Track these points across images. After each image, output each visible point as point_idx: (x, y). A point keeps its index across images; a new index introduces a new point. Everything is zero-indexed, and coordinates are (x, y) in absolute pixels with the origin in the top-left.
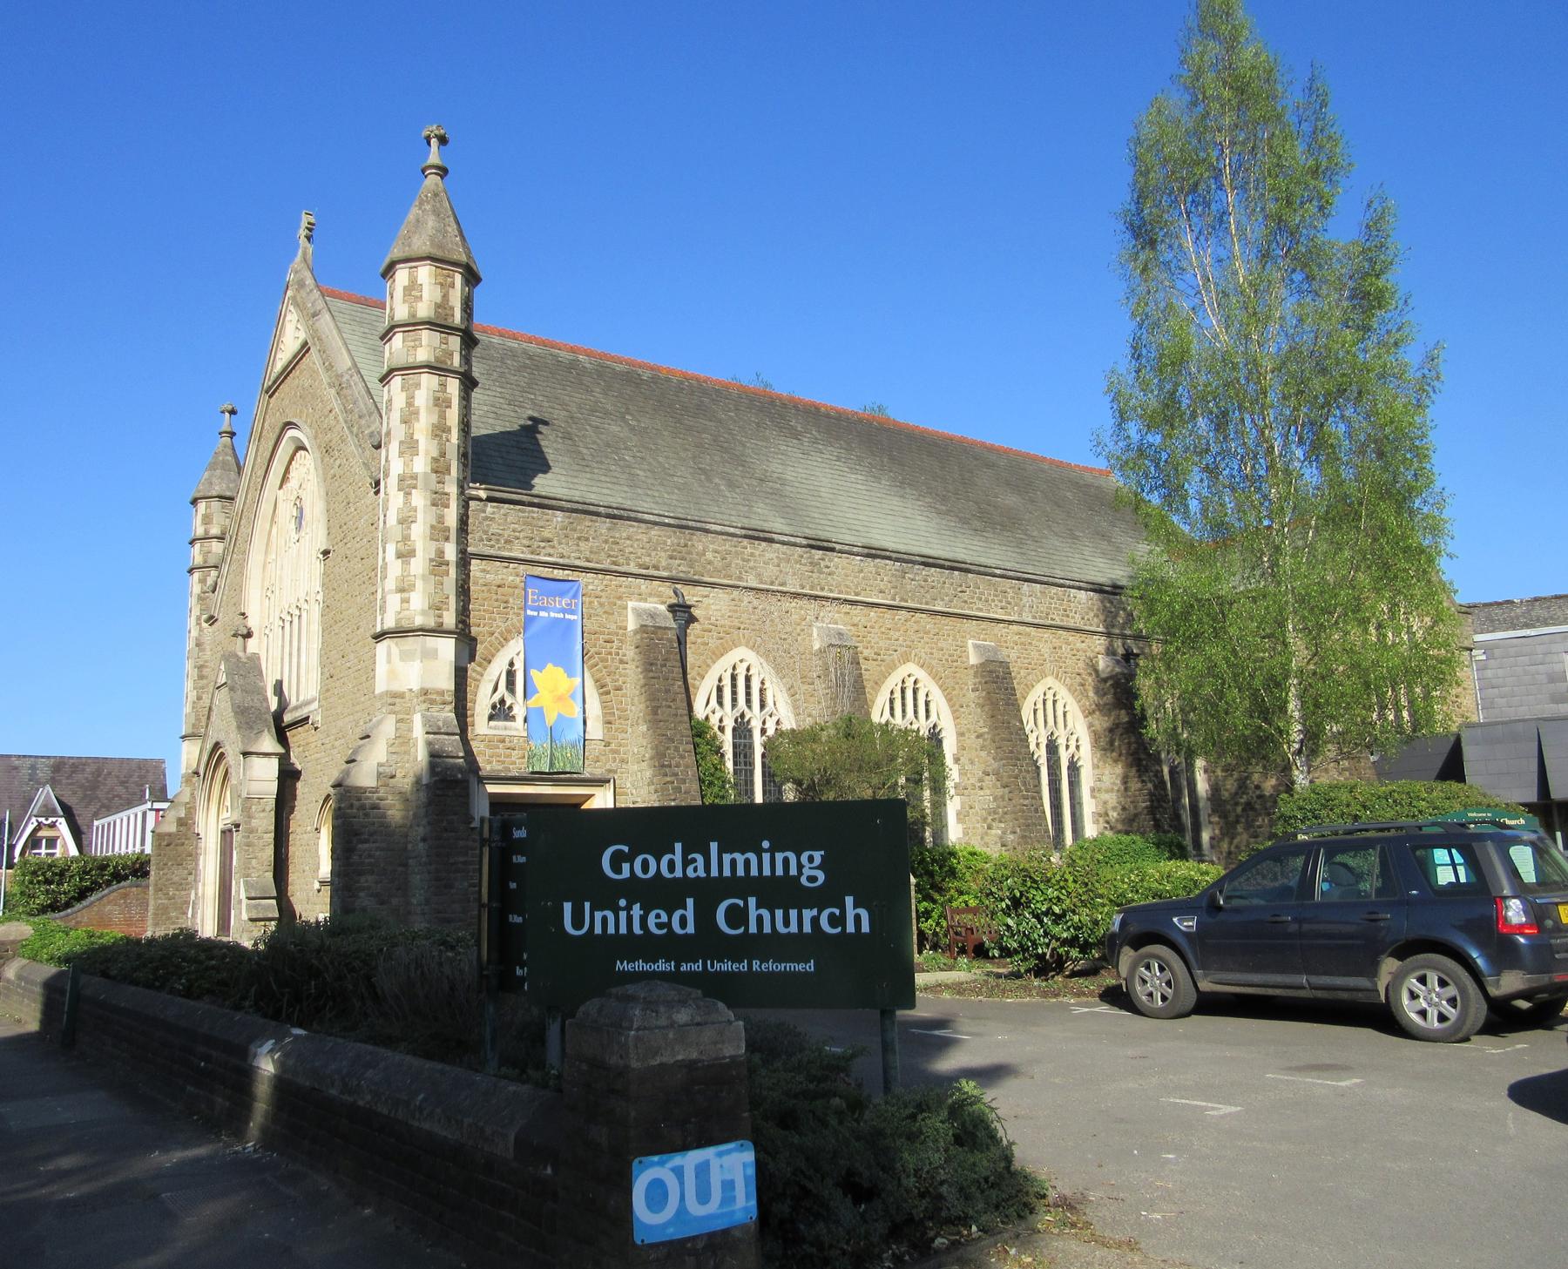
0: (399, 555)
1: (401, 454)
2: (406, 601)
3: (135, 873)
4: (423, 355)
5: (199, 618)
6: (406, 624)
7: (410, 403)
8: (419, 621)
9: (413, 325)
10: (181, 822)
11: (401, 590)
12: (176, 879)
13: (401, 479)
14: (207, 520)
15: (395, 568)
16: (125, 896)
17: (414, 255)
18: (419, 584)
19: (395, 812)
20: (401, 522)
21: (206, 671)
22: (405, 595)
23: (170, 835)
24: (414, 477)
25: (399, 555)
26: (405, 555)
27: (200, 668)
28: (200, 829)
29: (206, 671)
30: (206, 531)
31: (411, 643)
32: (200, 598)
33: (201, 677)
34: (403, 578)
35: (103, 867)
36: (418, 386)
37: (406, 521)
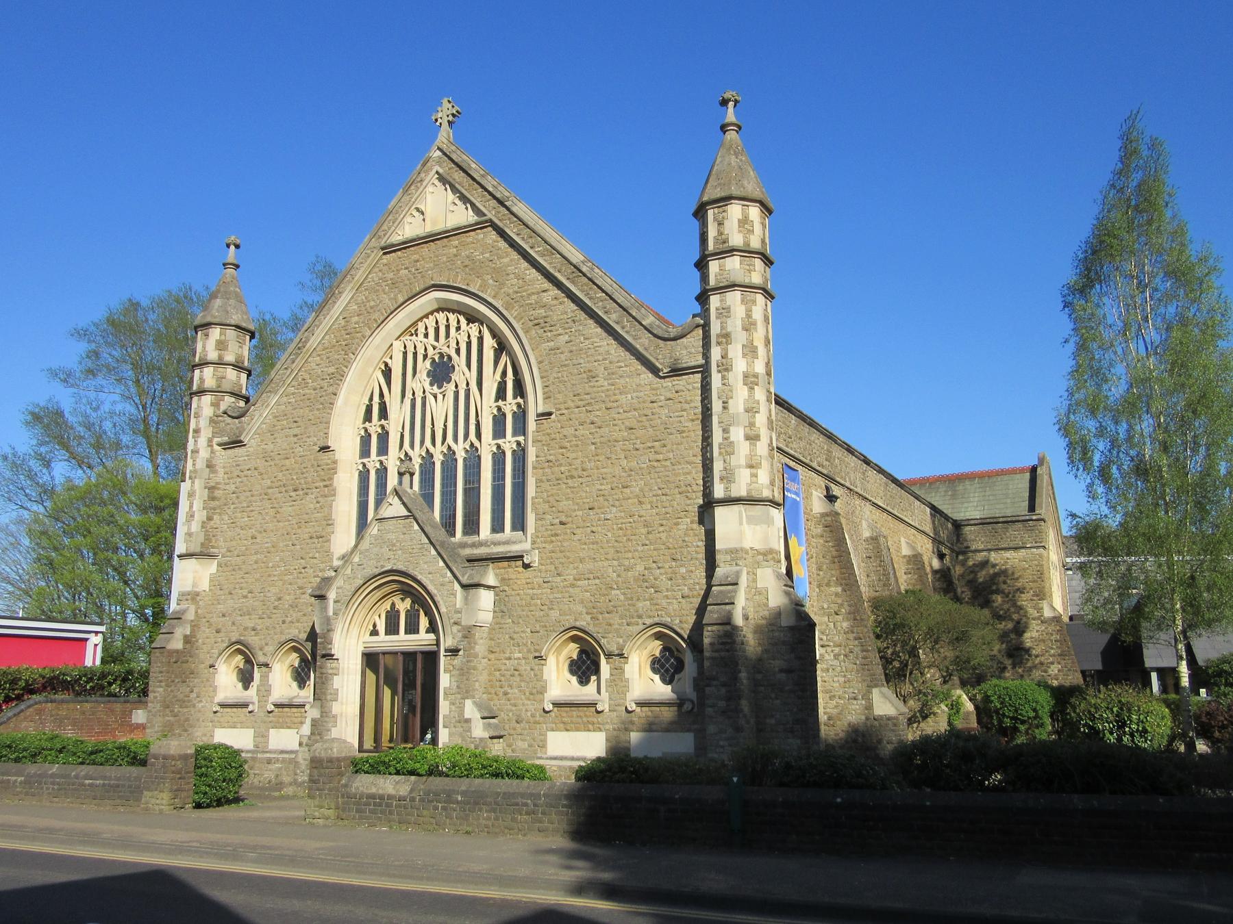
0: (748, 438)
1: (744, 355)
2: (755, 476)
3: (654, 727)
4: (756, 279)
5: (210, 441)
6: (755, 495)
7: (749, 315)
8: (766, 493)
9: (746, 252)
10: (187, 640)
11: (751, 467)
12: (181, 696)
13: (746, 376)
14: (221, 345)
15: (743, 448)
16: (39, 712)
17: (750, 196)
18: (765, 464)
19: (751, 642)
20: (747, 411)
21: (218, 493)
22: (754, 471)
23: (177, 651)
24: (756, 376)
25: (748, 438)
26: (752, 438)
27: (211, 489)
28: (336, 650)
29: (218, 493)
30: (220, 357)
31: (758, 510)
32: (211, 421)
33: (213, 498)
34: (751, 456)
35: (14, 682)
36: (754, 302)
37: (751, 410)
